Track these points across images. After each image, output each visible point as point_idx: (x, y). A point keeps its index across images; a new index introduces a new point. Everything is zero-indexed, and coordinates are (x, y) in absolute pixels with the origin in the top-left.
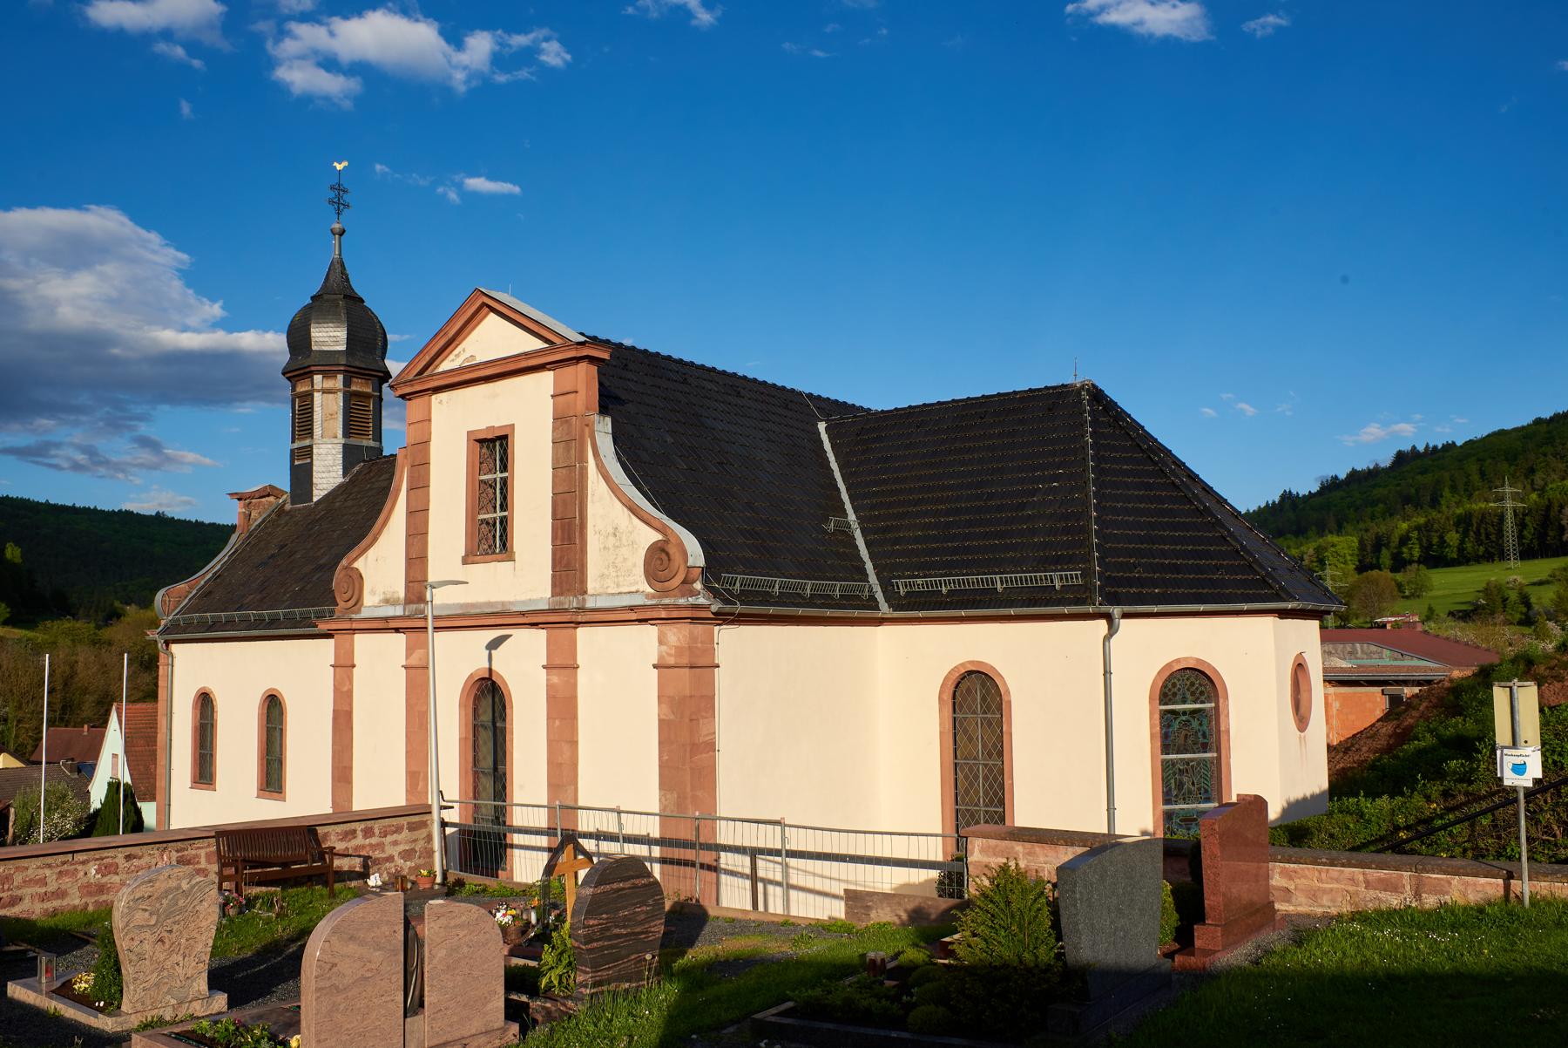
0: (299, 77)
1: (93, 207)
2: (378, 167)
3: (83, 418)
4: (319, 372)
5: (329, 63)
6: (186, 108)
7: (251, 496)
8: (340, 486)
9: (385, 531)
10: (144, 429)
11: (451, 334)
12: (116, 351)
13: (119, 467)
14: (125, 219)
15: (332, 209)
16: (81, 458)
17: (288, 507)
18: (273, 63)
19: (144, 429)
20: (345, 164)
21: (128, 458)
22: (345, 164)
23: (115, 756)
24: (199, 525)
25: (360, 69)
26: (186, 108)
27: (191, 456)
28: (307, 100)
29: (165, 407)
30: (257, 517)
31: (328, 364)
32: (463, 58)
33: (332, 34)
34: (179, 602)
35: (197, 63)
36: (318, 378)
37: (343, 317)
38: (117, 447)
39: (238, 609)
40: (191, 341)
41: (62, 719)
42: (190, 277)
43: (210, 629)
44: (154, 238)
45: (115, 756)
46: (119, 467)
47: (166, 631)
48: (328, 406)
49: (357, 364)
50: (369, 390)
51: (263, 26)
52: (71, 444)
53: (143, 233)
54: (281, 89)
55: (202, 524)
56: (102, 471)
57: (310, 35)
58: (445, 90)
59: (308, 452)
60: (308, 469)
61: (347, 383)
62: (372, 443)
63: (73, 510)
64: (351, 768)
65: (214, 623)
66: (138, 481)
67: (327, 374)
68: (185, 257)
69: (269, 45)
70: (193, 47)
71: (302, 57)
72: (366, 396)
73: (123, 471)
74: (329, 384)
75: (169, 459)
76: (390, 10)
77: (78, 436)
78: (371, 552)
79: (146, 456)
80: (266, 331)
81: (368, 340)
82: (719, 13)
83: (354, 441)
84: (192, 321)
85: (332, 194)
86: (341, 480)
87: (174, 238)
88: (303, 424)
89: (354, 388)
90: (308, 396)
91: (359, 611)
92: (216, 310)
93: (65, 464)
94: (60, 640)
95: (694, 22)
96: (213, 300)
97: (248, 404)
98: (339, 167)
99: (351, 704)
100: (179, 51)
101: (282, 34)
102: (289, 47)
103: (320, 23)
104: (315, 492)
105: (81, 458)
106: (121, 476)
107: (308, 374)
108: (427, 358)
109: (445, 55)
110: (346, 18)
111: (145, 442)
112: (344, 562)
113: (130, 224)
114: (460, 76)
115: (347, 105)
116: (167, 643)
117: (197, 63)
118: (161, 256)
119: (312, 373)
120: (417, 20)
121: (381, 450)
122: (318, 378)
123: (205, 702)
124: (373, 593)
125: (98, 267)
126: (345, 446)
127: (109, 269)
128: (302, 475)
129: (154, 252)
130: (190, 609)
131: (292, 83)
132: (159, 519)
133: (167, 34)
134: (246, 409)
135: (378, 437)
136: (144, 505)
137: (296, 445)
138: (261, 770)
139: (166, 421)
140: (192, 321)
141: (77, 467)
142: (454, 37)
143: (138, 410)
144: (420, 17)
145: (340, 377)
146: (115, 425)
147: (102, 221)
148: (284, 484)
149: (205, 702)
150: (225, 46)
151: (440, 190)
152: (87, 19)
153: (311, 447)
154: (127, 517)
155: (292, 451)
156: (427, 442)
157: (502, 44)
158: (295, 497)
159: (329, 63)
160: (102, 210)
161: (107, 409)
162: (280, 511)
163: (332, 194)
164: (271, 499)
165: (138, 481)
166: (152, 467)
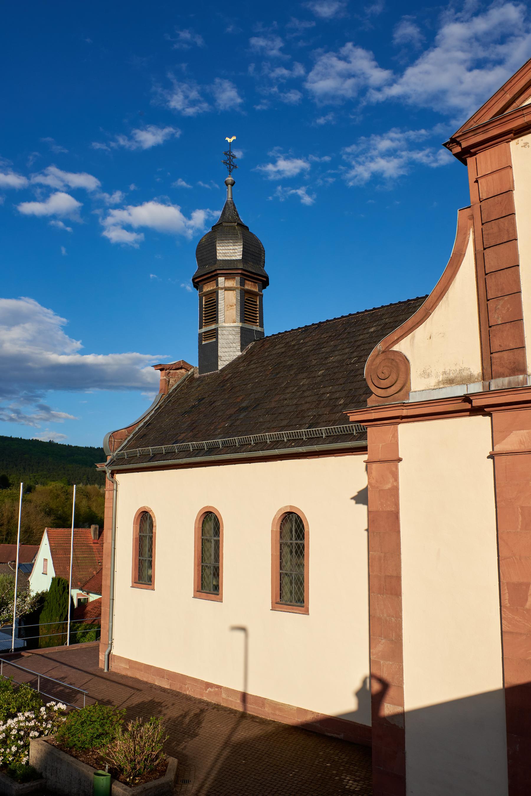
0: (115, 235)
1: (22, 297)
2: (151, 276)
3: (14, 396)
4: (222, 275)
5: (128, 228)
6: (63, 251)
7: (171, 367)
8: (239, 358)
9: (441, 303)
10: (42, 401)
11: (489, 106)
12: (30, 364)
13: (30, 420)
14: (36, 303)
15: (224, 168)
16: (13, 415)
17: (197, 375)
18: (103, 229)
19: (42, 401)
20: (234, 138)
21: (34, 416)
22: (234, 138)
23: (45, 560)
24: (69, 447)
25: (143, 230)
26: (63, 251)
27: (63, 414)
28: (118, 245)
29: (51, 391)
30: (174, 383)
31: (229, 269)
32: (191, 223)
33: (130, 214)
34: (121, 443)
35: (69, 229)
36: (221, 279)
37: (240, 236)
38: (30, 410)
39: (176, 442)
40: (64, 359)
41: (6, 539)
42: (67, 330)
43: (151, 459)
44: (50, 312)
45: (45, 560)
46: (30, 420)
47: (112, 463)
48: (228, 302)
49: (250, 269)
50: (257, 290)
51: (98, 212)
52: (9, 409)
53: (45, 310)
54: (107, 240)
55: (71, 446)
56: (23, 421)
57: (119, 215)
58: (183, 238)
59: (214, 334)
60: (215, 346)
61: (242, 283)
62: (259, 329)
63: (11, 439)
64: (399, 578)
65: (155, 455)
66: (39, 426)
67: (228, 276)
68: (64, 320)
69: (100, 220)
70: (67, 222)
71: (115, 225)
72: (255, 294)
73: (32, 422)
74: (230, 283)
75: (54, 416)
76: (155, 201)
77: (13, 405)
78: (420, 332)
79: (43, 414)
80: (99, 354)
81: (254, 252)
82: (315, 196)
83: (248, 326)
84: (67, 350)
85: (226, 158)
86: (240, 353)
87: (58, 312)
88: (210, 312)
89: (246, 287)
90: (215, 293)
91: (409, 399)
92: (78, 345)
93: (6, 418)
94: (6, 500)
95: (302, 201)
96: (77, 340)
97: (90, 389)
98: (229, 140)
99: (397, 504)
100: (61, 224)
101: (106, 215)
102: (110, 220)
103: (124, 209)
104: (220, 363)
105: (13, 415)
106: (31, 424)
107: (213, 277)
108: (508, 97)
109: (184, 222)
110: (135, 206)
111: (43, 408)
112: (379, 347)
113: (39, 305)
114: (190, 232)
115: (137, 246)
116: (112, 474)
117: (69, 229)
118: (53, 320)
119: (217, 275)
120: (169, 206)
121: (263, 333)
122: (221, 279)
123: (145, 519)
124: (426, 374)
125: (22, 325)
126: (242, 328)
127: (27, 326)
128: (208, 351)
129: (50, 318)
130: (128, 447)
131: (111, 239)
132: (51, 444)
133: (54, 217)
134: (90, 392)
135: (261, 325)
136: (44, 438)
137: (204, 330)
138: (134, 569)
139: (52, 397)
140: (67, 350)
141: (11, 419)
142: (187, 213)
143: (39, 392)
144: (170, 204)
145: (238, 278)
146: (29, 399)
147: (26, 304)
148: (194, 362)
149: (145, 519)
150: (80, 221)
151: (182, 285)
152: (19, 212)
153: (216, 330)
154: (36, 443)
155: (200, 335)
156: (509, 191)
157: (209, 215)
158: (202, 368)
159: (128, 228)
160: (27, 299)
161: (25, 392)
162: (191, 379)
163: (226, 158)
164: (183, 371)
165: (39, 426)
166: (47, 420)
